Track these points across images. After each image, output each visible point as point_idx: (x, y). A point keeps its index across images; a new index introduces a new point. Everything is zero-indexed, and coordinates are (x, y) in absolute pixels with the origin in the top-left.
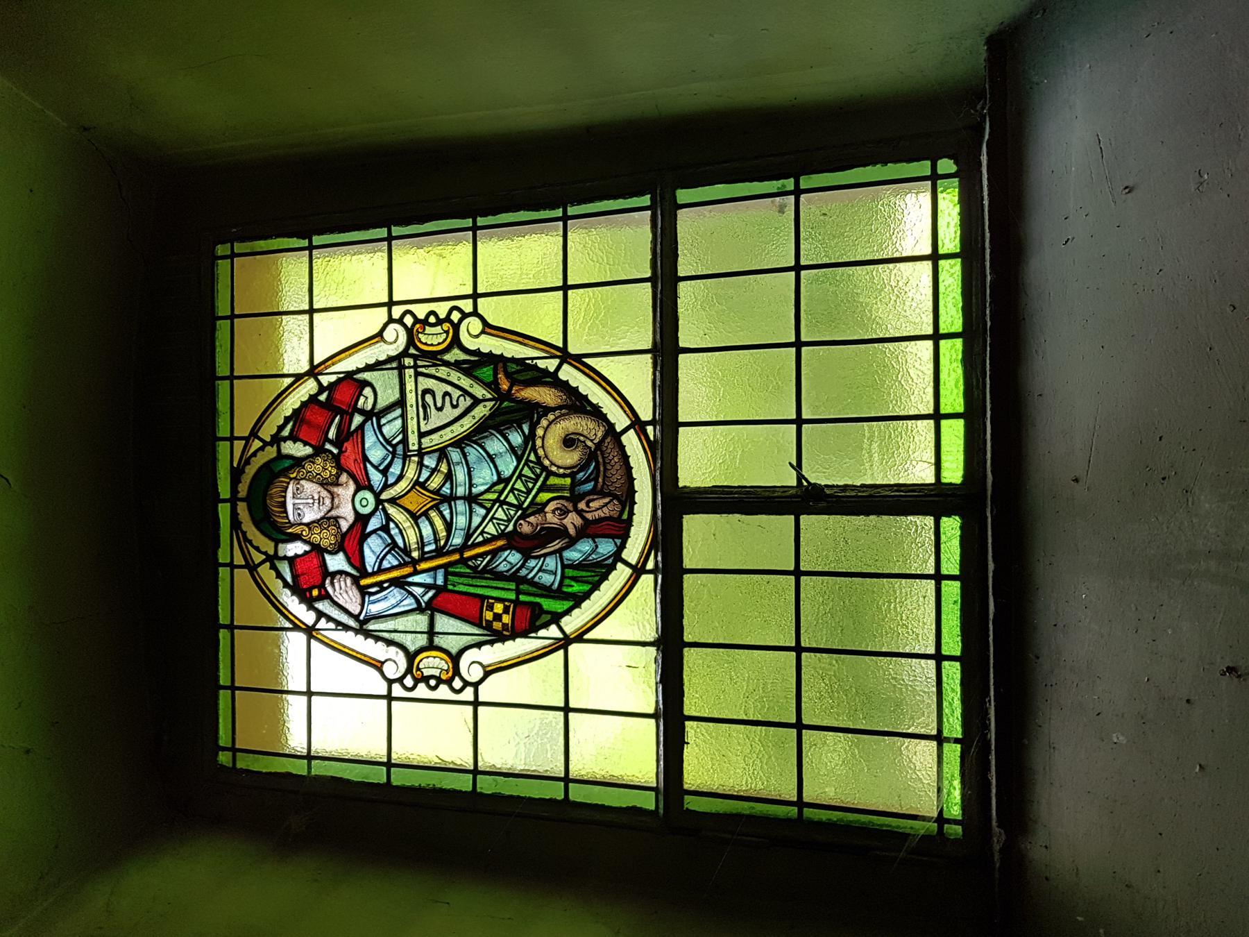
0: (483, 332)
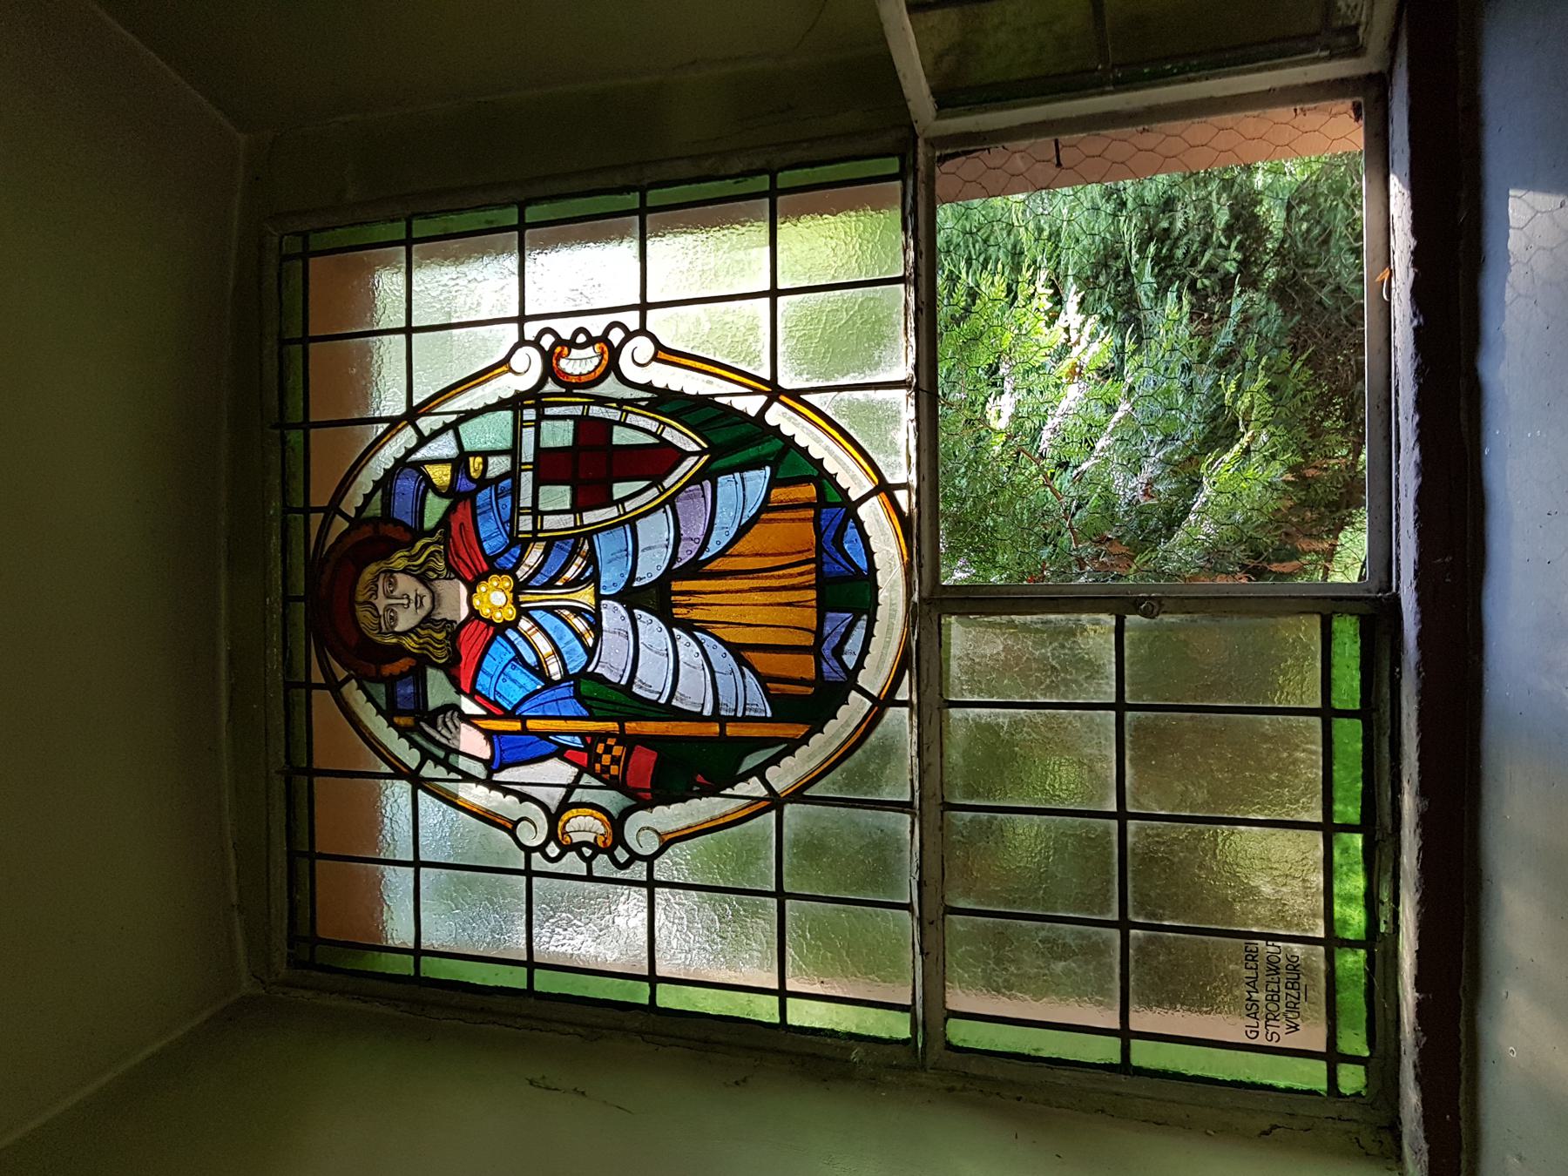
0: (655, 358)
